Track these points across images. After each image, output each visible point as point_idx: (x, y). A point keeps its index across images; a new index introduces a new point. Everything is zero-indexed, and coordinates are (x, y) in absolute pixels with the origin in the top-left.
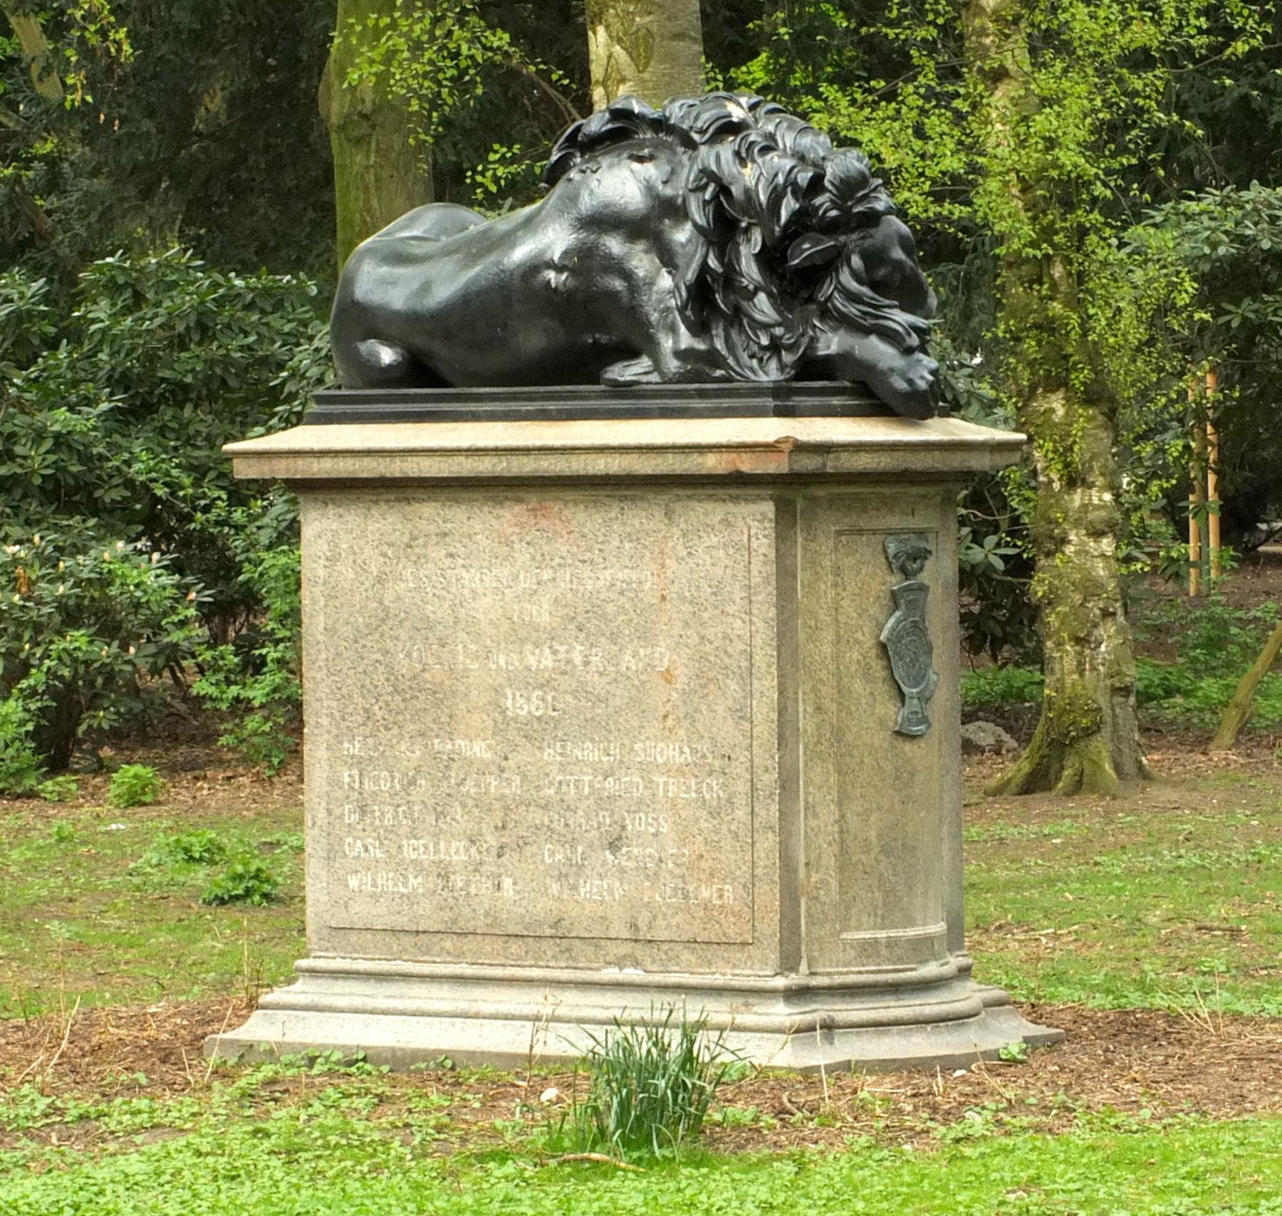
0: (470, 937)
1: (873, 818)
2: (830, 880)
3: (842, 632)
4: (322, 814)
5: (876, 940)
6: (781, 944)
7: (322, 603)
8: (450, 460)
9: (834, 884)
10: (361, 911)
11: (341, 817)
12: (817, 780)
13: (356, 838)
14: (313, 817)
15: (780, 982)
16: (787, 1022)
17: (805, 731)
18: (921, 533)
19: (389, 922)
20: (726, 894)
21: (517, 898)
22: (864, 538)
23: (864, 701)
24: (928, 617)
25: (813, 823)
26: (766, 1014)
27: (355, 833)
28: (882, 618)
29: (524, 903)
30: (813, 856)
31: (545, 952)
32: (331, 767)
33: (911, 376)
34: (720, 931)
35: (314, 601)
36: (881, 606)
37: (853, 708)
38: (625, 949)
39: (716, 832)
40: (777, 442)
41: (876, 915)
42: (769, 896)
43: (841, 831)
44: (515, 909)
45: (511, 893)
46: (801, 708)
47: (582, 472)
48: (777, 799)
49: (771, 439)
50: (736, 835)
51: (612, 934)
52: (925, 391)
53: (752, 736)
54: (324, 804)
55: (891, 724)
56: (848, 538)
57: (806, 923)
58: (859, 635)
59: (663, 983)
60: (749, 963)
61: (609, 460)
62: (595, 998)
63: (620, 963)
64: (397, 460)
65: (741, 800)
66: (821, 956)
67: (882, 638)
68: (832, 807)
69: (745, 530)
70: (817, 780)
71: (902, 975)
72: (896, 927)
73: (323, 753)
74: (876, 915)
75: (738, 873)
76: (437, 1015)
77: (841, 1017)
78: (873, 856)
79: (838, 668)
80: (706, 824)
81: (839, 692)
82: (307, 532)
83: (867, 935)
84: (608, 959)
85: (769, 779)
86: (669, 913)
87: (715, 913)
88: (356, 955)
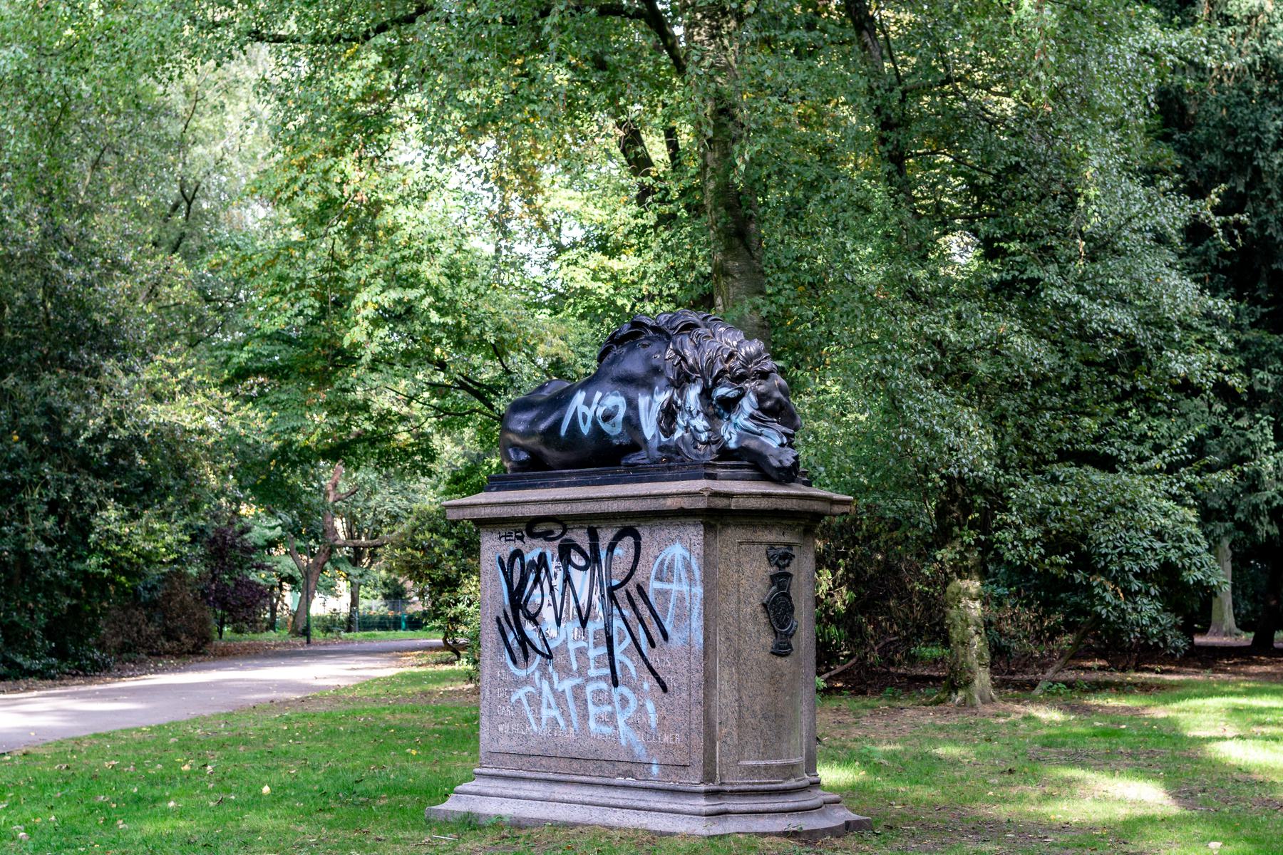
4: (488, 693)
9: (735, 734)
12: (726, 677)
15: (703, 787)
16: (704, 809)
19: (517, 749)
25: (724, 701)
28: (765, 590)
30: (724, 718)
38: (626, 767)
42: (698, 741)
50: (682, 708)
63: (625, 775)
65: (684, 688)
73: (488, 662)
82: (484, 547)
83: (754, 763)
85: (698, 676)
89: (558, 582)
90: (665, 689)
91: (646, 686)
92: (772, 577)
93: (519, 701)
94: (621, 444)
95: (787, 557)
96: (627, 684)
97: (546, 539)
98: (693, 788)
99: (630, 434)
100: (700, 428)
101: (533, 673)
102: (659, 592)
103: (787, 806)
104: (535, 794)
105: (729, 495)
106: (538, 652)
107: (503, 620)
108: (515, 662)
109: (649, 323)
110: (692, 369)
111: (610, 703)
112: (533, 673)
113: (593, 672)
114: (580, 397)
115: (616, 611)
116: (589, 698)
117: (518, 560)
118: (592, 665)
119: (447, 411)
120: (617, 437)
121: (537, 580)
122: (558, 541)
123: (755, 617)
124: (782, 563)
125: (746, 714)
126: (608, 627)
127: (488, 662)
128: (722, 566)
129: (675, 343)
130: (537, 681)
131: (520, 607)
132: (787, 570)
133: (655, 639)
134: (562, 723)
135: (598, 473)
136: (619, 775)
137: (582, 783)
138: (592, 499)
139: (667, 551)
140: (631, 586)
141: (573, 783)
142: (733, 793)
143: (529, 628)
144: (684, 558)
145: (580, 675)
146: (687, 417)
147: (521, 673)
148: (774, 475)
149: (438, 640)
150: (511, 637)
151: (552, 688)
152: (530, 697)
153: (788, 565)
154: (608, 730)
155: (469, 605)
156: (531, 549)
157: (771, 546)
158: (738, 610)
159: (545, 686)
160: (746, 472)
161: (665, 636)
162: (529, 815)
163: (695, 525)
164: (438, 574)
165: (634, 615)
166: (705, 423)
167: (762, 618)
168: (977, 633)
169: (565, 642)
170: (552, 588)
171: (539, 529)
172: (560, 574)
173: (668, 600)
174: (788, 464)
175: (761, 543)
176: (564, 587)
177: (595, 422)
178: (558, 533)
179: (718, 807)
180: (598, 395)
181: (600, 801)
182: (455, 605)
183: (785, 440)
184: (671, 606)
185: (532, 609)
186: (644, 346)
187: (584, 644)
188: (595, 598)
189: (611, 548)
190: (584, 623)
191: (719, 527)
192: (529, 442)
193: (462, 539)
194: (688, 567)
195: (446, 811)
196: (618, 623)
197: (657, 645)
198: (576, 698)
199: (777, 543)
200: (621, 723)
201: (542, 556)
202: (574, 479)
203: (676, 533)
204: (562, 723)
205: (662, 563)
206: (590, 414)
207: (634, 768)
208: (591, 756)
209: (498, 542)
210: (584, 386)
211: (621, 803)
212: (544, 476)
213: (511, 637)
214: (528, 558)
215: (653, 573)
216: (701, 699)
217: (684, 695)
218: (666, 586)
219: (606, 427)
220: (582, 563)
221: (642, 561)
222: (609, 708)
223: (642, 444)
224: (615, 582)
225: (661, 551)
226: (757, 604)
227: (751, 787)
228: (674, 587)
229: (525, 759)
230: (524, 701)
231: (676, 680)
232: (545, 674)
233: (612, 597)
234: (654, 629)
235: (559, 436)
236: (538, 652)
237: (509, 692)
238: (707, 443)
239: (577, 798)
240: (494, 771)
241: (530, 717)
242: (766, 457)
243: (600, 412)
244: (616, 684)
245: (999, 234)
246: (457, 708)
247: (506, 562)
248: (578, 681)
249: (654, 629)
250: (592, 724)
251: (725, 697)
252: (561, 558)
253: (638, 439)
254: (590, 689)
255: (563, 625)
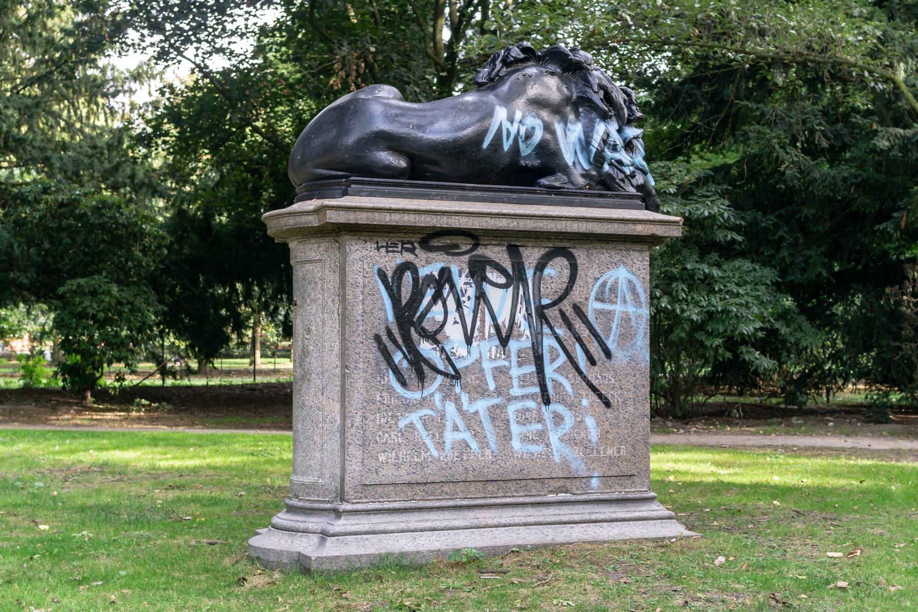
8: (480, 220)
10: (388, 474)
13: (384, 433)
19: (407, 479)
27: (384, 429)
32: (367, 392)
35: (355, 297)
45: (490, 457)
51: (554, 476)
63: (557, 491)
64: (445, 218)
76: (458, 528)
77: (332, 529)
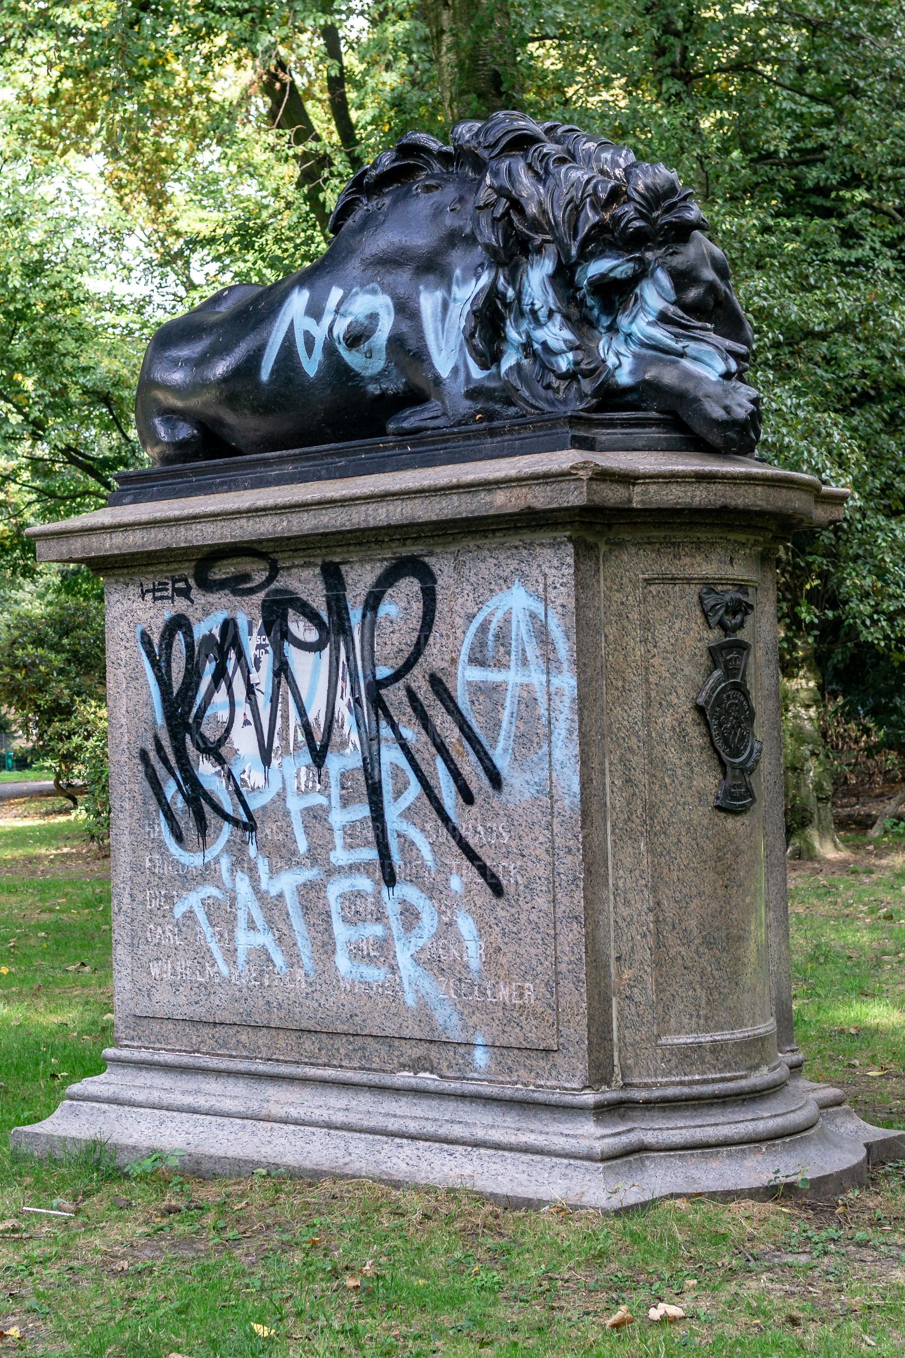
0: (265, 1030)
1: (693, 906)
2: (645, 977)
3: (653, 694)
4: (126, 900)
5: (700, 1045)
6: (590, 1051)
7: (124, 686)
9: (649, 981)
11: (143, 903)
12: (628, 862)
14: (120, 902)
15: (589, 1098)
16: (599, 1147)
17: (614, 808)
18: (742, 587)
20: (527, 993)
21: (310, 990)
22: (677, 588)
23: (679, 772)
24: (748, 678)
25: (625, 911)
26: (574, 1136)
28: (699, 679)
29: (316, 995)
30: (625, 949)
31: (338, 1050)
33: (728, 402)
34: (520, 1034)
36: (697, 665)
37: (667, 780)
38: (419, 1051)
39: (515, 922)
40: (572, 468)
41: (698, 1016)
43: (657, 921)
44: (308, 1002)
45: (304, 986)
46: (608, 780)
47: (363, 525)
48: (581, 884)
49: (566, 466)
51: (406, 1033)
52: (746, 420)
53: (552, 813)
54: (128, 890)
55: (711, 798)
56: (660, 588)
57: (619, 1026)
58: (673, 698)
59: (459, 1092)
60: (554, 1073)
61: (391, 508)
62: (391, 1105)
63: (416, 1066)
65: (541, 886)
66: (636, 1064)
67: (701, 701)
68: (646, 893)
69: (541, 579)
70: (628, 862)
71: (731, 1085)
72: (722, 1029)
74: (698, 1016)
75: (539, 968)
78: (693, 948)
79: (649, 735)
80: (504, 913)
81: (651, 762)
84: (402, 1060)
85: (571, 863)
86: (466, 1012)
87: (515, 1015)
88: (158, 1045)
89: (263, 678)
90: (497, 889)
91: (455, 883)
92: (711, 651)
93: (190, 915)
94: (383, 394)
95: (741, 609)
96: (415, 880)
97: (235, 592)
98: (568, 1099)
99: (402, 371)
100: (556, 344)
101: (217, 860)
102: (478, 689)
103: (763, 1126)
104: (228, 1105)
105: (628, 479)
106: (226, 817)
107: (153, 756)
108: (179, 838)
109: (435, 145)
110: (535, 225)
111: (380, 917)
112: (217, 860)
113: (340, 856)
114: (299, 300)
115: (386, 731)
116: (335, 907)
117: (179, 636)
118: (339, 841)
119: (52, 495)
120: (375, 379)
121: (220, 674)
122: (262, 595)
123: (682, 735)
124: (731, 621)
125: (671, 939)
126: (370, 765)
127: (126, 839)
128: (611, 631)
129: (496, 174)
130: (225, 875)
131: (187, 728)
132: (742, 635)
133: (473, 787)
134: (279, 959)
135: (338, 453)
136: (403, 1066)
137: (325, 1082)
138: (332, 503)
139: (493, 602)
140: (418, 679)
141: (305, 1081)
142: (649, 1105)
143: (206, 769)
144: (533, 616)
145: (314, 861)
146: (525, 325)
147: (193, 860)
148: (715, 438)
149: (49, 783)
150: (170, 789)
151: (256, 890)
152: (211, 908)
153: (741, 625)
154: (375, 974)
155: (87, 738)
156: (206, 613)
157: (709, 585)
158: (647, 722)
159: (243, 885)
160: (653, 433)
161: (495, 779)
162: (217, 1151)
163: (555, 545)
164: (44, 701)
165: (424, 738)
166: (567, 334)
167: (696, 736)
168: (813, 754)
169: (281, 796)
170: (250, 690)
171: (219, 573)
172: (267, 661)
173: (498, 705)
174: (741, 413)
175: (689, 581)
176: (276, 687)
177: (330, 350)
178: (259, 577)
179: (624, 1139)
180: (336, 294)
181: (367, 1123)
182: (69, 737)
183: (733, 366)
184: (505, 716)
185: (210, 732)
186: (428, 189)
187: (322, 800)
188: (342, 706)
189: (373, 602)
190: (319, 756)
191: (603, 548)
192: (194, 402)
193: (75, 653)
194: (542, 635)
195: (49, 1137)
196: (391, 755)
197: (479, 799)
198: (306, 910)
199: (721, 581)
200: (404, 959)
201: (228, 626)
202: (289, 468)
203: (513, 564)
204: (279, 959)
205: (484, 628)
206: (320, 333)
207: (434, 1053)
208: (341, 1028)
209: (138, 604)
210: (305, 279)
211: (413, 1127)
212: (228, 468)
213: (170, 789)
214: (200, 631)
215: (465, 650)
216: (580, 910)
217: (542, 902)
218: (493, 676)
219: (352, 358)
220: (312, 636)
221: (439, 627)
222: (378, 930)
223: (429, 388)
224: (383, 672)
225: (480, 604)
226: (686, 706)
227: (686, 1090)
228: (512, 677)
229: (206, 1031)
230: (201, 916)
231: (522, 870)
232: (240, 862)
233: (378, 704)
234: (470, 766)
235: (257, 383)
236: (226, 817)
237: (169, 898)
238: (571, 376)
239: (320, 1114)
240: (144, 1055)
241: (214, 946)
242: (696, 400)
243: (340, 329)
244: (390, 879)
245: (835, 179)
246: (71, 882)
247: (156, 639)
248: (309, 874)
249: (470, 766)
250: (342, 962)
251: (627, 903)
252: (267, 628)
253: (421, 380)
254: (335, 890)
255: (275, 762)
